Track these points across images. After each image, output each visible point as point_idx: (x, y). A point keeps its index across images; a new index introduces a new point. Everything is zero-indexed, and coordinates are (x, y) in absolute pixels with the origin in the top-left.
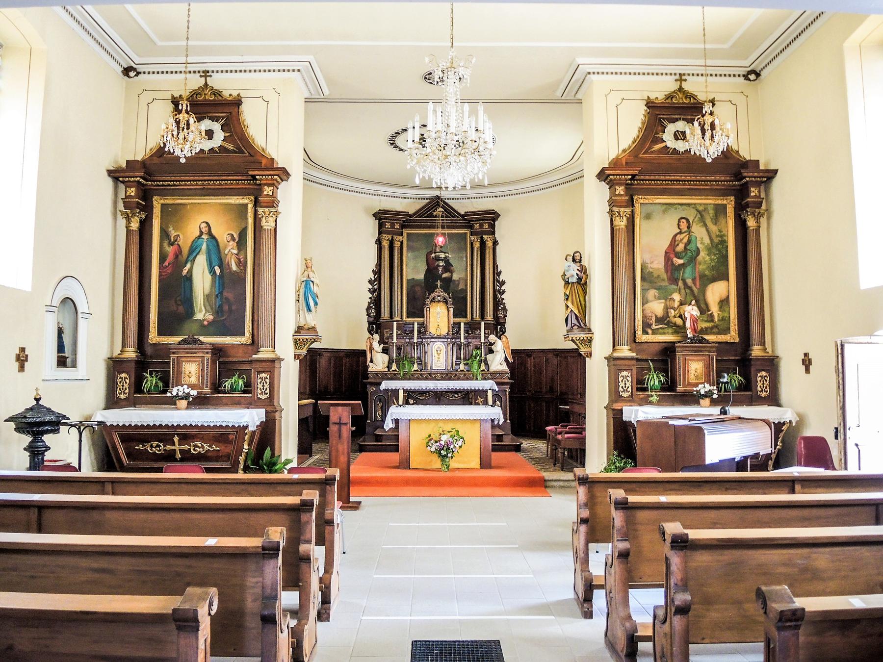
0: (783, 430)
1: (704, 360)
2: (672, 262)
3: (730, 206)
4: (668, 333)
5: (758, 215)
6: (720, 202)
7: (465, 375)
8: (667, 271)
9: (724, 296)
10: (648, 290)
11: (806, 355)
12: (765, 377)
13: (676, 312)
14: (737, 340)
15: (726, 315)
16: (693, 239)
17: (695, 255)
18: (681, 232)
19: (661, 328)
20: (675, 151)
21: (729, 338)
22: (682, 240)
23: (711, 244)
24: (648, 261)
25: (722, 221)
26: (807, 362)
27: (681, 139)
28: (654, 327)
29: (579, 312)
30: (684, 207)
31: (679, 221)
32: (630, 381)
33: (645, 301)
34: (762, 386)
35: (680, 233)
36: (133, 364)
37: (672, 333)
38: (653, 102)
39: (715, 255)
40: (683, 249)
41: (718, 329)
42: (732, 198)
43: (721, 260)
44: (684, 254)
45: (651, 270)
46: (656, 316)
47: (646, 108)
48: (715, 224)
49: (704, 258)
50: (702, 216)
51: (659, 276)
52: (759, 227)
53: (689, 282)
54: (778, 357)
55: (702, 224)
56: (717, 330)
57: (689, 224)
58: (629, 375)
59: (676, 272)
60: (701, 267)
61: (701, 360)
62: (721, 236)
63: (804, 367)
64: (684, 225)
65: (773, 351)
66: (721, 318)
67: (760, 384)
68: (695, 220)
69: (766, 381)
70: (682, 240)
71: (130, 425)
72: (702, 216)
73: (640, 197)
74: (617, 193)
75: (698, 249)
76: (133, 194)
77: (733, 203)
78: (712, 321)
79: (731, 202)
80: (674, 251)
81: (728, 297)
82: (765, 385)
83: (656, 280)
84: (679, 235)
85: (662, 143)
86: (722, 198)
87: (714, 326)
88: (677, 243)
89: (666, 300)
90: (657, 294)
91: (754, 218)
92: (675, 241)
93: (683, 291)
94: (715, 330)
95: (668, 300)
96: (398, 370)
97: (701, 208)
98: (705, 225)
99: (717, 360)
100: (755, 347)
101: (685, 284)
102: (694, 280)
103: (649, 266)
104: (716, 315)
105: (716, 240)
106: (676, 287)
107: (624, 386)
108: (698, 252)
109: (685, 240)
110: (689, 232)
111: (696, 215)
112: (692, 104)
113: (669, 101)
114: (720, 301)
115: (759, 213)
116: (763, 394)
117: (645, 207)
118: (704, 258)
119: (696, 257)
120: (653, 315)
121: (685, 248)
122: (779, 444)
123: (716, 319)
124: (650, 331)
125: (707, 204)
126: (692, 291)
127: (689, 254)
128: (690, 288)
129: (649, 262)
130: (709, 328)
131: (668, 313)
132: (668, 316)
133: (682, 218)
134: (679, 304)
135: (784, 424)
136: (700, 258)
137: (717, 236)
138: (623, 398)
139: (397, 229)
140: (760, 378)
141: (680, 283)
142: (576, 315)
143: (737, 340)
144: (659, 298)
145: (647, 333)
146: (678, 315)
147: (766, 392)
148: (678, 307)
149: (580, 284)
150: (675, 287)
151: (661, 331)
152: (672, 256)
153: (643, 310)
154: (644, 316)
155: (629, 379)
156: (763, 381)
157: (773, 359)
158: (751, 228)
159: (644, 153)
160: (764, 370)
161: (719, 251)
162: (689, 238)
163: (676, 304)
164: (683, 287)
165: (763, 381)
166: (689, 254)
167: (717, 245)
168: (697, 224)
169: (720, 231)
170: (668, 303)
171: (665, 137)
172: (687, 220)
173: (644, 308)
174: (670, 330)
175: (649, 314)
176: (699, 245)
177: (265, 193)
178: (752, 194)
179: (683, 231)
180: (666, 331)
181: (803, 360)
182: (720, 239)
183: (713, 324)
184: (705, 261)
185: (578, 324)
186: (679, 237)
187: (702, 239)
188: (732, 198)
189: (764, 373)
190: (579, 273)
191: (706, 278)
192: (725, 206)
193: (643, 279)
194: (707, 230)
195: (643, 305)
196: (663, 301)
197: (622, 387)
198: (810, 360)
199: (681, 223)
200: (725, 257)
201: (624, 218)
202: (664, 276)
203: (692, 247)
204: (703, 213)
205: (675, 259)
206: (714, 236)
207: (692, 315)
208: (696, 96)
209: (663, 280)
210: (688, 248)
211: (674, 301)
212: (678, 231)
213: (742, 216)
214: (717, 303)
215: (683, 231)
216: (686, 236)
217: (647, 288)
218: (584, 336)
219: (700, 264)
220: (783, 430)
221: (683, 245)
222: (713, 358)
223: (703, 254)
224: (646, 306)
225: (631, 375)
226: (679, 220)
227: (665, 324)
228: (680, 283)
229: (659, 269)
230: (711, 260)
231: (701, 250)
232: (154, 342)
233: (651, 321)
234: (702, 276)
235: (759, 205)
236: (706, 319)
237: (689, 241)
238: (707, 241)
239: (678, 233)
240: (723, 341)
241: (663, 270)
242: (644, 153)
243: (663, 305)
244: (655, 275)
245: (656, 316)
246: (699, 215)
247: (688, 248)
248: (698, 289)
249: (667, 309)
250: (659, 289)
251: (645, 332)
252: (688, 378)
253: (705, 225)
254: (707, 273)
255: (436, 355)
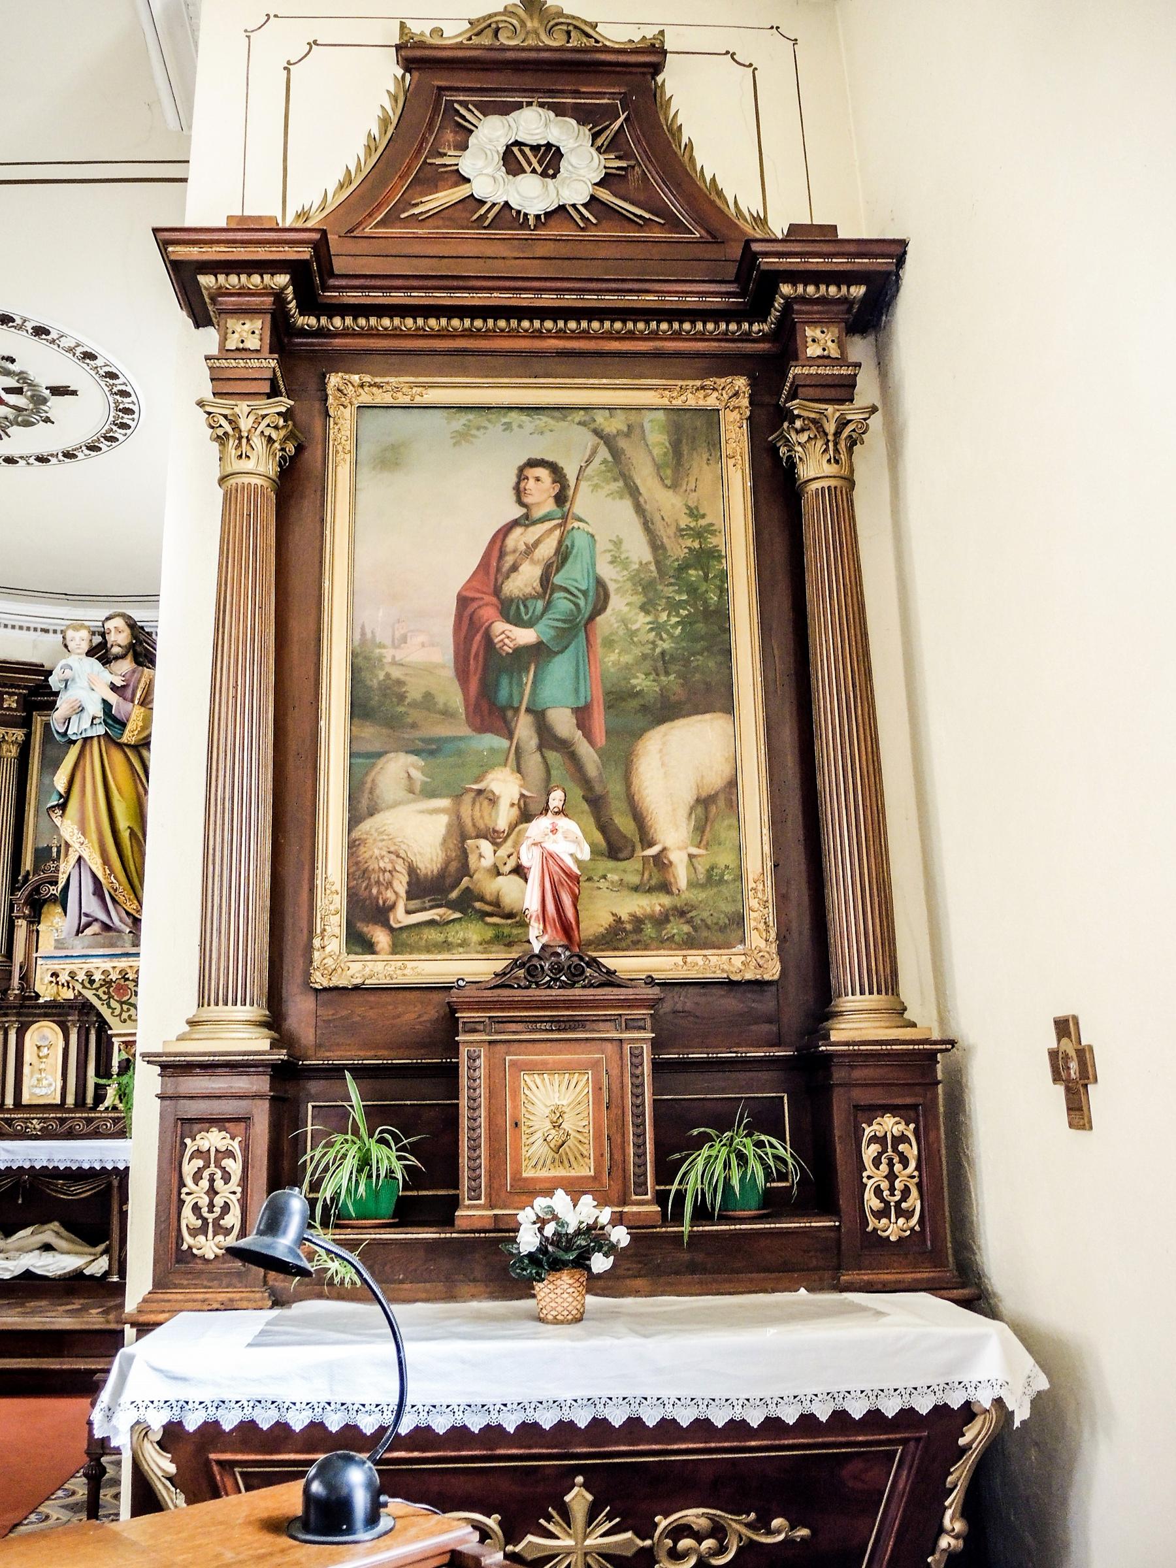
0: (963, 1450)
1: (595, 1065)
2: (488, 640)
3: (735, 415)
4: (464, 944)
5: (837, 434)
6: (693, 400)
7: (63, 1121)
8: (462, 673)
9: (715, 780)
10: (379, 755)
11: (1064, 1027)
12: (203, 1230)
13: (503, 852)
14: (773, 971)
15: (725, 859)
16: (580, 541)
17: (587, 611)
18: (527, 516)
19: (431, 923)
20: (507, 215)
21: (738, 961)
22: (530, 550)
23: (658, 563)
24: (383, 636)
25: (701, 470)
26: (1074, 1065)
27: (534, 171)
28: (400, 917)
29: (106, 861)
30: (543, 420)
31: (521, 476)
32: (236, 1177)
33: (364, 802)
34: (885, 1185)
35: (525, 521)
36: (261, 1084)
37: (486, 944)
38: (421, 45)
39: (673, 606)
40: (537, 584)
41: (689, 922)
42: (741, 382)
43: (700, 627)
44: (540, 605)
45: (396, 673)
46: (412, 871)
47: (399, 72)
48: (674, 486)
49: (624, 622)
50: (616, 453)
51: (428, 696)
52: (850, 482)
53: (563, 722)
54: (953, 1043)
55: (621, 484)
56: (686, 928)
57: (564, 487)
58: (235, 1146)
59: (504, 682)
60: (612, 660)
61: (581, 1068)
62: (699, 534)
63: (1060, 1089)
64: (541, 489)
65: (942, 1021)
66: (702, 877)
67: (874, 1177)
68: (589, 471)
69: (905, 1162)
70: (530, 550)
71: (634, 1423)
72: (616, 453)
73: (355, 378)
74: (232, 344)
75: (600, 583)
76: (253, 343)
77: (745, 402)
78: (665, 887)
79: (734, 402)
80: (497, 592)
81: (732, 784)
82: (898, 1184)
83: (415, 715)
84: (518, 531)
85: (456, 185)
86: (698, 383)
87: (675, 908)
88: (509, 560)
89: (458, 798)
90: (416, 774)
91: (820, 443)
92: (502, 554)
93: (533, 761)
94: (677, 928)
95: (468, 798)
96: (121, 1106)
97: (613, 425)
98: (633, 491)
99: (657, 1066)
100: (850, 1002)
101: (547, 737)
102: (582, 715)
103: (388, 654)
104: (678, 858)
105: (678, 550)
106: (504, 743)
107: (204, 1201)
108: (601, 596)
109: (547, 549)
110: (565, 518)
111: (594, 452)
112: (574, 50)
113: (486, 40)
114: (698, 801)
115: (843, 424)
116: (894, 1229)
117: (375, 423)
118: (624, 622)
119: (592, 618)
120: (401, 867)
121: (545, 580)
122: (947, 1522)
123: (681, 875)
124: (381, 938)
125: (639, 409)
126: (573, 757)
127: (562, 604)
128: (565, 747)
129: (388, 642)
130: (652, 918)
131: (464, 854)
132: (465, 870)
133: (532, 463)
134: (515, 812)
135: (968, 1412)
136: (606, 622)
137: (681, 532)
138: (200, 1266)
139: (9, 709)
140: (874, 1149)
141: (524, 728)
142: (94, 876)
143: (773, 971)
144: (430, 792)
145: (368, 947)
146: (511, 863)
147: (908, 1215)
148: (512, 827)
149: (120, 746)
150: (501, 743)
151: (432, 935)
152: (488, 613)
153: (353, 846)
154: (357, 871)
155: (234, 1167)
156: (891, 1164)
157: (932, 1056)
158: (814, 486)
159: (382, 223)
160: (893, 1110)
161: (692, 590)
162: (560, 542)
163: (504, 817)
164: (534, 742)
165: (891, 1164)
166: (562, 604)
167: (683, 568)
168: (596, 487)
169: (693, 513)
170: (466, 811)
171: (467, 164)
172: (555, 469)
173: (354, 835)
174: (474, 932)
175: (375, 854)
176: (606, 571)
177: (813, 351)
178: (813, 351)
179: (537, 513)
180: (456, 934)
181: (1053, 1055)
182: (696, 545)
183: (667, 900)
184: (633, 634)
185: (102, 916)
186: (518, 539)
187: (618, 543)
188: (741, 382)
189: (889, 1125)
190: (113, 698)
191: (634, 703)
192: (711, 416)
193: (359, 709)
194: (639, 509)
195: (354, 820)
196: (445, 803)
197: (196, 1208)
198: (1084, 1056)
199: (531, 484)
200: (720, 617)
201: (257, 441)
202: (453, 697)
203: (573, 575)
204: (622, 443)
205: (500, 628)
206: (666, 535)
207: (549, 857)
208: (594, 26)
209: (447, 714)
210: (558, 580)
211: (493, 801)
212: (517, 512)
213: (783, 450)
214: (683, 812)
215: (537, 513)
216: (551, 530)
217: (376, 747)
218: (107, 965)
219: (609, 643)
220: (963, 1450)
221: (537, 571)
222: (636, 1055)
223: (621, 604)
224: (366, 826)
225: (246, 1148)
226: (521, 470)
227: (452, 905)
228: (524, 728)
229: (429, 669)
230: (657, 628)
231: (612, 587)
232: (339, 981)
233: (390, 895)
234: (618, 697)
235: (843, 390)
236: (635, 879)
237: (563, 555)
238: (639, 550)
239: (515, 523)
240: (709, 975)
241: (449, 672)
242: (382, 223)
243: (443, 820)
244: (414, 693)
245: (412, 871)
246: (604, 453)
247: (558, 580)
248: (601, 753)
249: (464, 837)
250: (432, 753)
251: (359, 942)
252: (517, 1160)
253: (633, 491)
254: (640, 681)
255: (35, 1060)
